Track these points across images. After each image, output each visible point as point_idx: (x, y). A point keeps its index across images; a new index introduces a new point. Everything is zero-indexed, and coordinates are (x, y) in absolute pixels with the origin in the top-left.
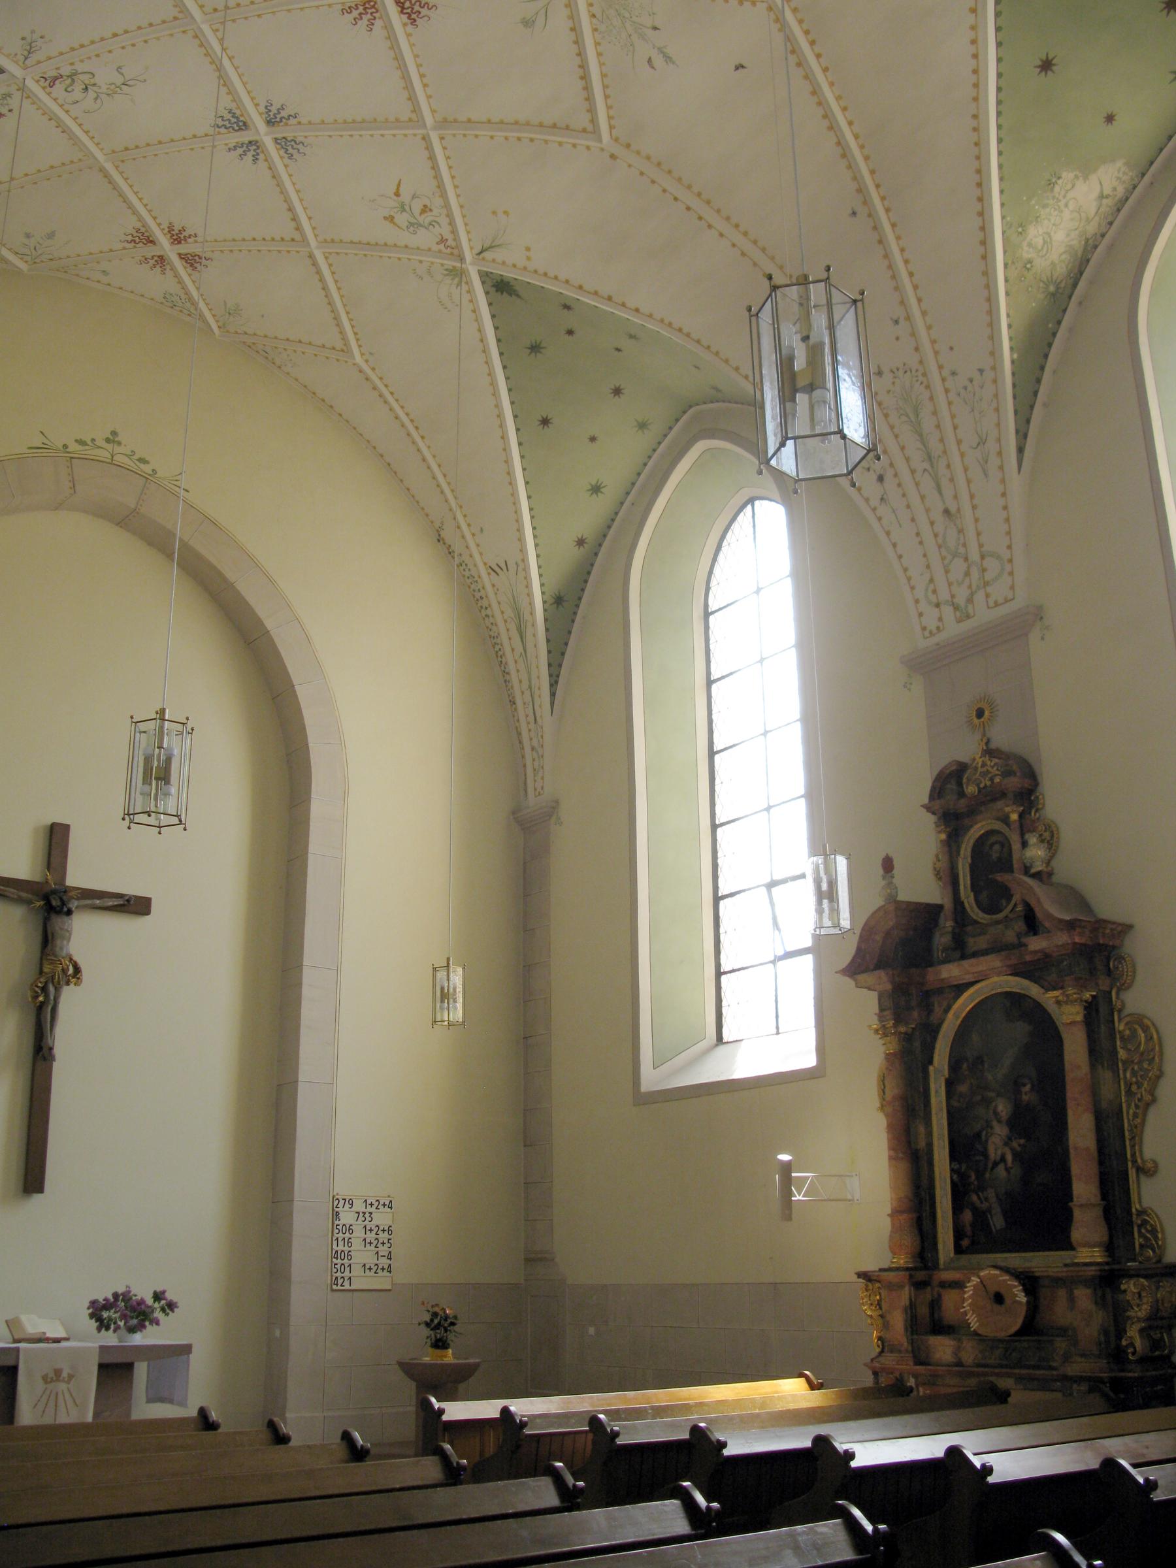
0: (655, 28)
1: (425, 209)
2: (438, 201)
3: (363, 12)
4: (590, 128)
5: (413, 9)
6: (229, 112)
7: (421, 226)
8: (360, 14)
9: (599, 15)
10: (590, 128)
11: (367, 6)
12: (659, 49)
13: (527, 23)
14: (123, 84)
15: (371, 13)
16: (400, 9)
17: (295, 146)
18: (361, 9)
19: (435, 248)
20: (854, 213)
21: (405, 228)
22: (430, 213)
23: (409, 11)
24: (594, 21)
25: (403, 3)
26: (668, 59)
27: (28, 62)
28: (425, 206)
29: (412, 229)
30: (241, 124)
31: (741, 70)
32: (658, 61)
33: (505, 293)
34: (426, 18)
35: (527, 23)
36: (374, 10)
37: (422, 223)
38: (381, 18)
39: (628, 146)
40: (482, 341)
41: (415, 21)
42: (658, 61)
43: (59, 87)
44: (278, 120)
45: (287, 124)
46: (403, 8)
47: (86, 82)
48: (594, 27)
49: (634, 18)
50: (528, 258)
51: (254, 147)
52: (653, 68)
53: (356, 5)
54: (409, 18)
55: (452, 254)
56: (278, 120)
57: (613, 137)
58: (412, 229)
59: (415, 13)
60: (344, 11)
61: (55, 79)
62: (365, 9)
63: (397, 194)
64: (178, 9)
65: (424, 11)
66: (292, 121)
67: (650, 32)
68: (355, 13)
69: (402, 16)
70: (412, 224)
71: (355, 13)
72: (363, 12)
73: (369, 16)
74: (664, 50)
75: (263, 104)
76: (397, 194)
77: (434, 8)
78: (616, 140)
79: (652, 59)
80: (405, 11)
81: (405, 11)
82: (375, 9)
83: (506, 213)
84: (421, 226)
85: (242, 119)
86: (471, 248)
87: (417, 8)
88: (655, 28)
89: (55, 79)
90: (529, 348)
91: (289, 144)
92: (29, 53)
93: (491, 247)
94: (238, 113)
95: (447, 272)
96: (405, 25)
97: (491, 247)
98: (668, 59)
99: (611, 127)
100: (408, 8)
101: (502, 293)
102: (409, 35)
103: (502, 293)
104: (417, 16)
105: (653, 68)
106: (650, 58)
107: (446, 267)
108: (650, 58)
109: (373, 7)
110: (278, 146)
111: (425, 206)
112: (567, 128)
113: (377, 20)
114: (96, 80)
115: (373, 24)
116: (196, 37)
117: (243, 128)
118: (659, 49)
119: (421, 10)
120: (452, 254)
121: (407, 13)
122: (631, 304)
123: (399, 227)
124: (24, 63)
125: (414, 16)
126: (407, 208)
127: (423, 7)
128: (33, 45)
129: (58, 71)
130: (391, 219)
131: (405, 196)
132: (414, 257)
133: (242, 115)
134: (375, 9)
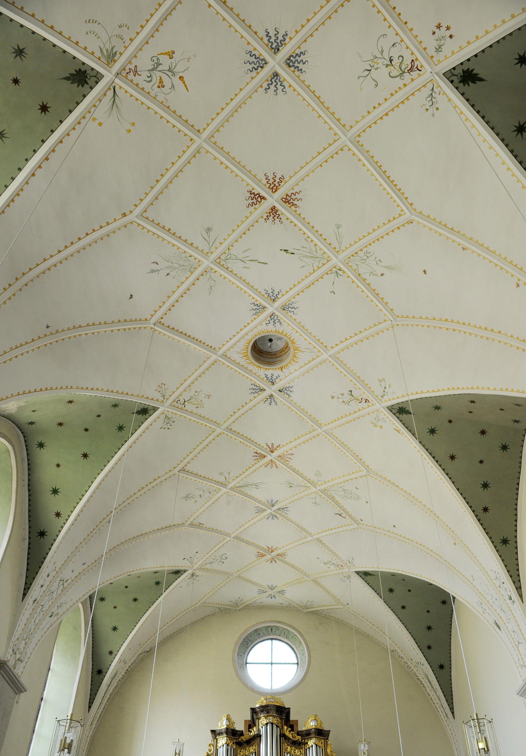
0: (168, 274)
1: (161, 85)
2: (161, 98)
3: (274, 183)
4: (145, 215)
5: (256, 199)
6: (301, 70)
7: (153, 69)
8: (275, 181)
9: (189, 258)
10: (145, 215)
11: (275, 188)
12: (159, 270)
13: (209, 230)
14: (370, 70)
15: (271, 185)
16: (261, 195)
17: (253, 65)
18: (276, 183)
19: (135, 62)
20: (48, 327)
21: (159, 57)
22: (157, 84)
23: (257, 197)
24: (189, 255)
25: (261, 199)
26: (153, 271)
27: (430, 86)
28: (163, 86)
29: (156, 61)
30: (291, 64)
31: (130, 297)
32: (155, 267)
33: (75, 73)
34: (247, 199)
35: (209, 230)
36: (271, 187)
37: (154, 72)
38: (265, 185)
39: (125, 226)
40: (52, 27)
41: (251, 194)
42: (155, 267)
43: (407, 62)
44: (273, 80)
45: (267, 80)
46: (260, 196)
47: (392, 68)
48: (186, 253)
49: (177, 270)
50: (94, 119)
51: (274, 46)
52: (153, 263)
53: (280, 184)
54: (254, 193)
55: (124, 69)
56: (273, 80)
57: (133, 222)
58: (156, 61)
59: (253, 197)
60: (283, 178)
61: (411, 70)
62: (275, 185)
63: (181, 78)
64: (360, 143)
65: (250, 201)
66: (265, 85)
67: (168, 271)
68: (277, 180)
69: (258, 193)
70: (159, 64)
71: (277, 180)
72: (274, 183)
73: (271, 182)
74: (157, 272)
75: (287, 89)
76: (181, 78)
77: (248, 206)
78: (132, 223)
79: (157, 265)
80: (258, 195)
81: (258, 195)
82: (271, 188)
83: (129, 131)
84: (153, 69)
85: (292, 69)
86: (121, 87)
87: (254, 201)
88: (168, 274)
89: (411, 70)
90: (23, 49)
91: (258, 64)
92: (432, 94)
93: (114, 101)
94: (297, 73)
95: (114, 52)
96: (253, 189)
97: (114, 101)
98: (153, 271)
99: (139, 225)
100: (258, 197)
101: (76, 71)
102: (248, 185)
103: (76, 71)
104: (251, 197)
105: (153, 263)
106: (158, 264)
107: (118, 55)
108: (158, 264)
109: (272, 189)
110: (261, 57)
111: (163, 86)
112: (152, 204)
113: (266, 183)
114: (386, 71)
115: (266, 179)
116: (344, 126)
117: (288, 61)
118: (159, 270)
119: (250, 195)
120: (124, 69)
121: (256, 195)
122: (39, 172)
123: (162, 54)
124: (433, 84)
125: (253, 196)
126: (170, 74)
127: (252, 203)
128: (431, 102)
129: (411, 77)
130: (171, 55)
131: (176, 80)
132: (390, 485)
133: (294, 71)
134: (271, 188)
